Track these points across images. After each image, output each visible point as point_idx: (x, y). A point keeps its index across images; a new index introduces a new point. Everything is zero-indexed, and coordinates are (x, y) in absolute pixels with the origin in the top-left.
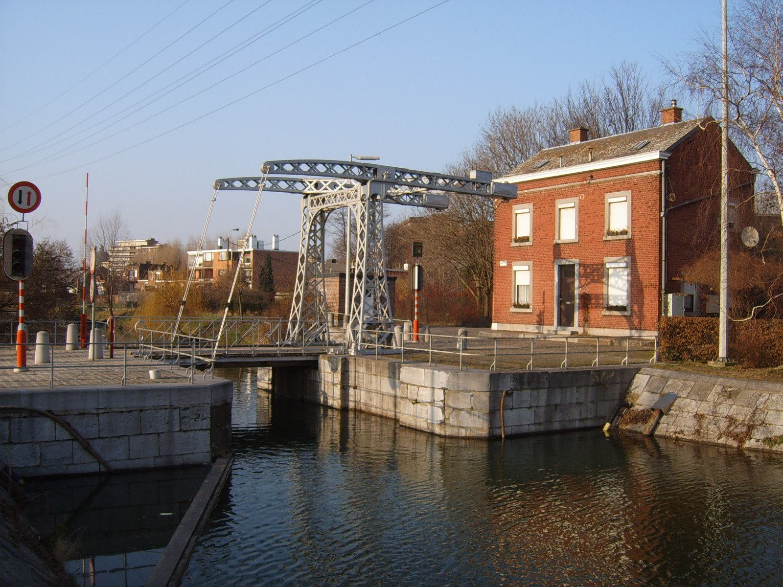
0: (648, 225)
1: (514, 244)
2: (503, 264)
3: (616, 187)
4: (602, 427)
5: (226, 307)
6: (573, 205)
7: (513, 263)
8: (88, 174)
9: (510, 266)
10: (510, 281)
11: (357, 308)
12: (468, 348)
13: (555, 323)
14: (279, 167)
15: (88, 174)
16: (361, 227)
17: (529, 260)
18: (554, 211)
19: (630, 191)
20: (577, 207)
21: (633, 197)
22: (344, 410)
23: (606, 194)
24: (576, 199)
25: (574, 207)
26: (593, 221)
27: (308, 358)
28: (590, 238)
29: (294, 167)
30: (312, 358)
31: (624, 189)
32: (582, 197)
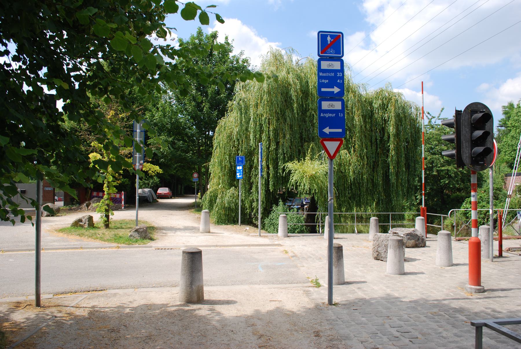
8: (422, 82)
15: (422, 82)
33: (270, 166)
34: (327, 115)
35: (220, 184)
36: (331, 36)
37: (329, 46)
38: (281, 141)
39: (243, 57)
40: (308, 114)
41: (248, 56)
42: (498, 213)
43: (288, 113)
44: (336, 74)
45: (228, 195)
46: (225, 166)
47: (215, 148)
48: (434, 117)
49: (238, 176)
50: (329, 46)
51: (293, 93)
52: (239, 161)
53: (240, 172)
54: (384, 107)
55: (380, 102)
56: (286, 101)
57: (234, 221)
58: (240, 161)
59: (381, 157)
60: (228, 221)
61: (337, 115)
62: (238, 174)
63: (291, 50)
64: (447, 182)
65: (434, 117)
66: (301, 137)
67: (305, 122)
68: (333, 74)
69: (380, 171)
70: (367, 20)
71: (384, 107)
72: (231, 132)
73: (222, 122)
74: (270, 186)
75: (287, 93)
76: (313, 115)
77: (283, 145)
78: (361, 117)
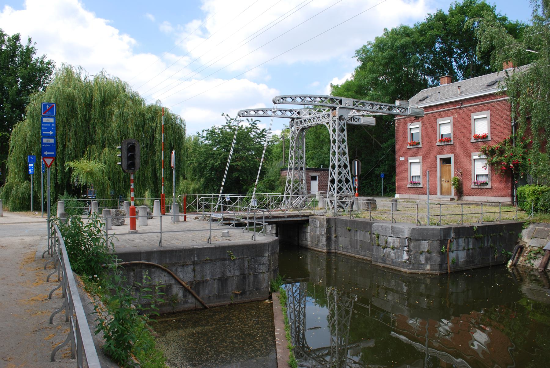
0: (503, 131)
1: (408, 147)
2: (402, 159)
3: (479, 109)
4: (507, 263)
5: (61, 184)
6: (449, 121)
7: (409, 158)
9: (406, 160)
10: (407, 169)
11: (289, 186)
12: (480, 215)
13: (439, 193)
14: (283, 100)
16: (333, 136)
17: (419, 156)
18: (436, 125)
19: (489, 111)
20: (452, 123)
21: (491, 114)
22: (329, 253)
23: (472, 114)
24: (451, 118)
25: (450, 123)
26: (463, 131)
27: (303, 219)
28: (461, 141)
29: (293, 100)
30: (306, 218)
31: (485, 110)
32: (455, 116)
33: (58, 164)
34: (46, 146)
35: (16, 178)
36: (49, 105)
37: (48, 110)
38: (68, 144)
39: (46, 60)
40: (92, 122)
41: (51, 59)
42: (270, 199)
43: (73, 122)
44: (51, 125)
45: (22, 187)
46: (20, 163)
47: (11, 148)
48: (233, 119)
49: (30, 172)
50: (48, 110)
51: (77, 106)
52: (30, 160)
53: (31, 168)
54: (153, 119)
55: (150, 115)
56: (72, 111)
57: (28, 209)
58: (32, 160)
59: (151, 157)
60: (23, 208)
61: (51, 145)
62: (30, 170)
63: (80, 68)
64: (237, 175)
65: (233, 119)
66: (85, 141)
67: (89, 128)
68: (49, 125)
69: (149, 167)
70: (202, 8)
71: (153, 119)
72: (26, 135)
73: (19, 125)
74: (58, 179)
75: (73, 105)
76: (96, 123)
77: (68, 147)
78: (134, 126)
